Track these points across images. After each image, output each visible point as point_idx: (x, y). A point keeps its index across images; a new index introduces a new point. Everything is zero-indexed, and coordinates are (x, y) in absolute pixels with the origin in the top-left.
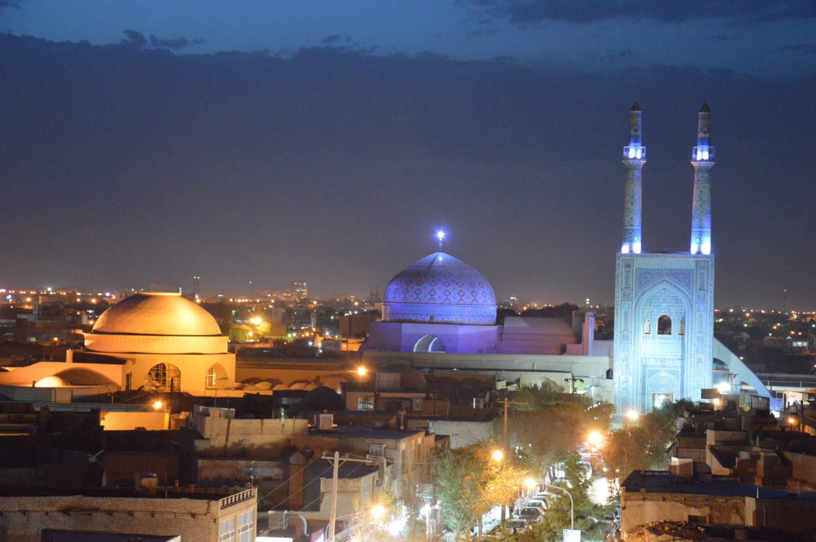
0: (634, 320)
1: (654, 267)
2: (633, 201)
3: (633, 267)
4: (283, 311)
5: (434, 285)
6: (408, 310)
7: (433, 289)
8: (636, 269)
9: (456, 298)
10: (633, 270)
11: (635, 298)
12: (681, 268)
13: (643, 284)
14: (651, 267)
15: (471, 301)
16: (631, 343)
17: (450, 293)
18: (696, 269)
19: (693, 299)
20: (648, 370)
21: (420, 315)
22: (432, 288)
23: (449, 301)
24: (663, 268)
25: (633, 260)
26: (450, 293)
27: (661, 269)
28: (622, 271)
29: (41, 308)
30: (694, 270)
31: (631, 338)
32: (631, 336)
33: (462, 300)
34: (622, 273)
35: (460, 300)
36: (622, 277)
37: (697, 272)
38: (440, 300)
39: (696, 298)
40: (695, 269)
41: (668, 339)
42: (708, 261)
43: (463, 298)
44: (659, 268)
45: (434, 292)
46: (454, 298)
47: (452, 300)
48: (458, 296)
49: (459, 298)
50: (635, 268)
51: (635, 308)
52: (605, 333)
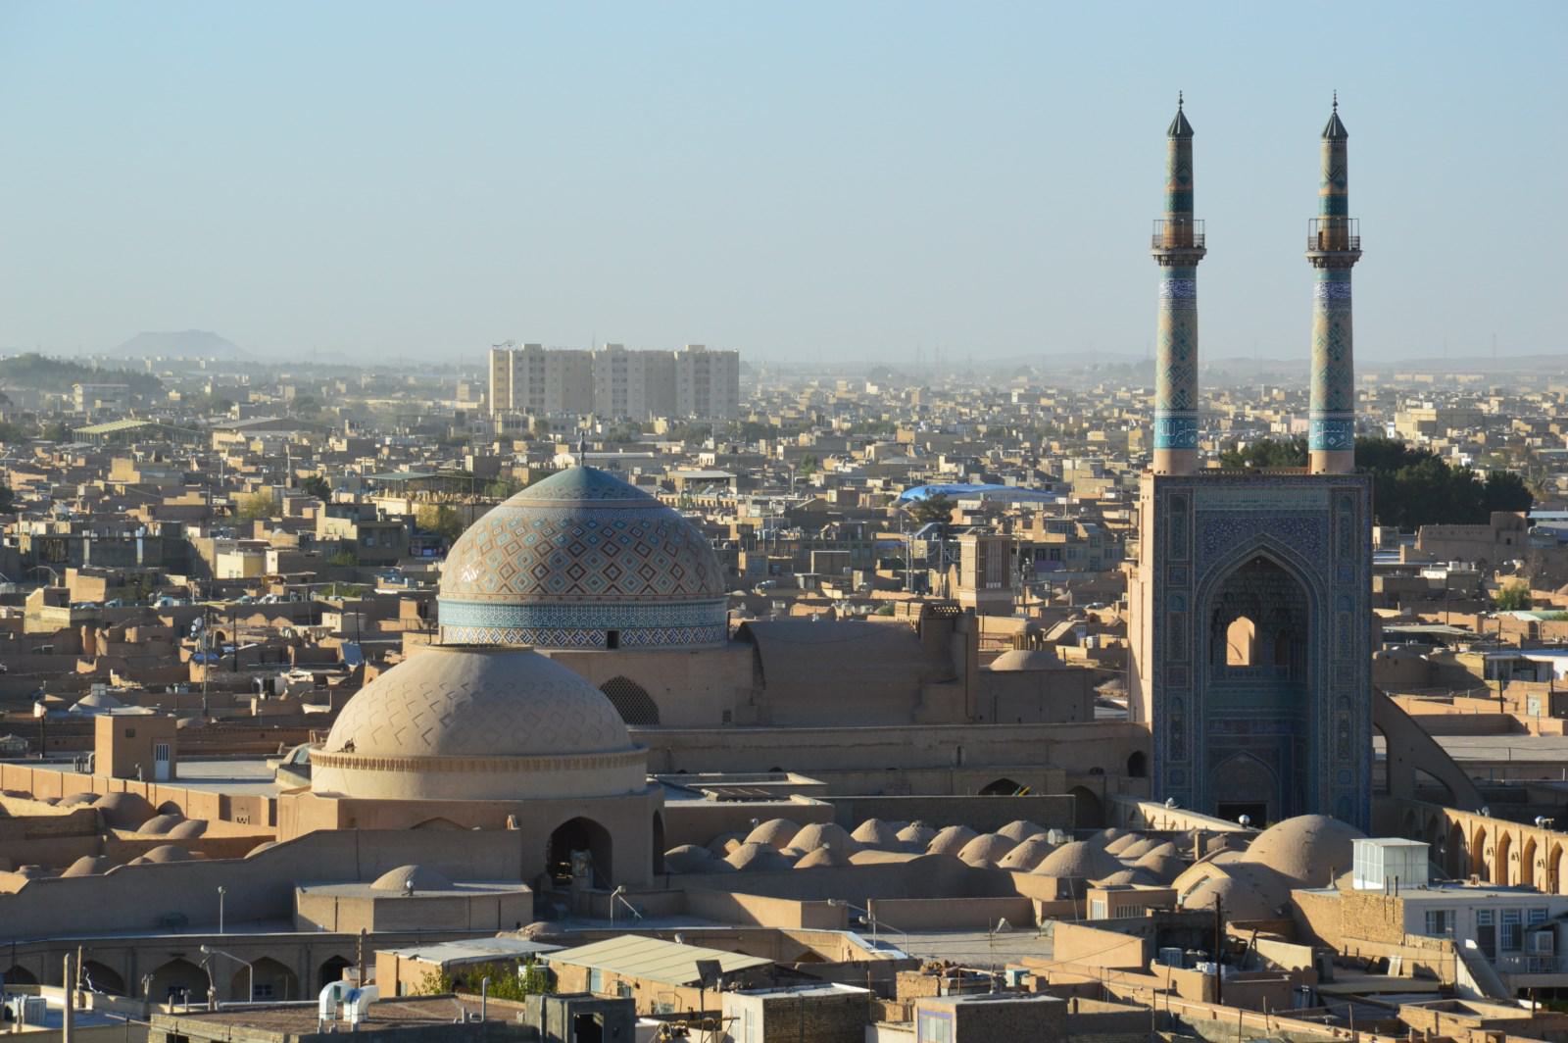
0: (1196, 634)
1: (1237, 506)
2: (1185, 349)
3: (1191, 509)
4: (921, 605)
5: (615, 554)
6: (637, 618)
7: (612, 564)
8: (1197, 512)
9: (668, 583)
10: (1191, 517)
11: (1197, 583)
12: (1299, 509)
13: (1215, 548)
14: (1231, 506)
15: (696, 589)
16: (1189, 690)
17: (654, 572)
18: (1333, 508)
19: (1326, 581)
20: (1172, 759)
21: (584, 630)
22: (612, 560)
23: (653, 593)
24: (1259, 509)
25: (1192, 492)
26: (654, 572)
27: (1255, 512)
28: (1166, 519)
29: (1525, 596)
30: (1327, 511)
31: (1190, 677)
32: (1190, 673)
33: (613, 589)
34: (1166, 525)
35: (609, 589)
36: (1166, 534)
37: (1334, 516)
38: (632, 590)
39: (1333, 579)
40: (1330, 509)
41: (342, 763)
42: (1358, 490)
43: (681, 582)
44: (1251, 509)
45: (616, 572)
46: (664, 583)
47: (659, 589)
48: (671, 577)
49: (607, 583)
50: (1194, 509)
51: (1197, 606)
52: (441, 720)
